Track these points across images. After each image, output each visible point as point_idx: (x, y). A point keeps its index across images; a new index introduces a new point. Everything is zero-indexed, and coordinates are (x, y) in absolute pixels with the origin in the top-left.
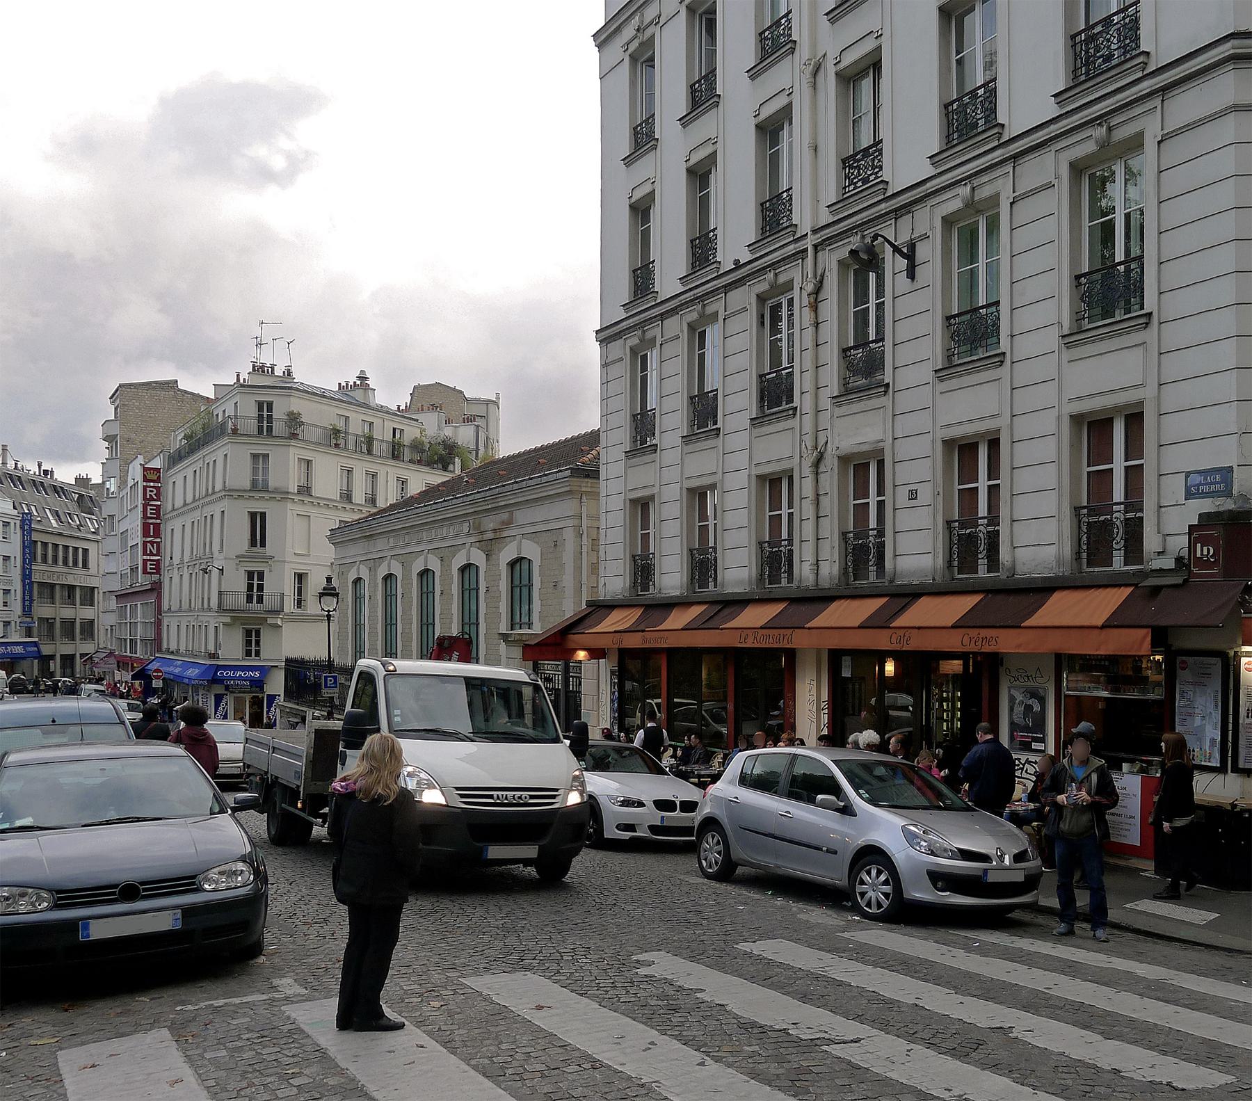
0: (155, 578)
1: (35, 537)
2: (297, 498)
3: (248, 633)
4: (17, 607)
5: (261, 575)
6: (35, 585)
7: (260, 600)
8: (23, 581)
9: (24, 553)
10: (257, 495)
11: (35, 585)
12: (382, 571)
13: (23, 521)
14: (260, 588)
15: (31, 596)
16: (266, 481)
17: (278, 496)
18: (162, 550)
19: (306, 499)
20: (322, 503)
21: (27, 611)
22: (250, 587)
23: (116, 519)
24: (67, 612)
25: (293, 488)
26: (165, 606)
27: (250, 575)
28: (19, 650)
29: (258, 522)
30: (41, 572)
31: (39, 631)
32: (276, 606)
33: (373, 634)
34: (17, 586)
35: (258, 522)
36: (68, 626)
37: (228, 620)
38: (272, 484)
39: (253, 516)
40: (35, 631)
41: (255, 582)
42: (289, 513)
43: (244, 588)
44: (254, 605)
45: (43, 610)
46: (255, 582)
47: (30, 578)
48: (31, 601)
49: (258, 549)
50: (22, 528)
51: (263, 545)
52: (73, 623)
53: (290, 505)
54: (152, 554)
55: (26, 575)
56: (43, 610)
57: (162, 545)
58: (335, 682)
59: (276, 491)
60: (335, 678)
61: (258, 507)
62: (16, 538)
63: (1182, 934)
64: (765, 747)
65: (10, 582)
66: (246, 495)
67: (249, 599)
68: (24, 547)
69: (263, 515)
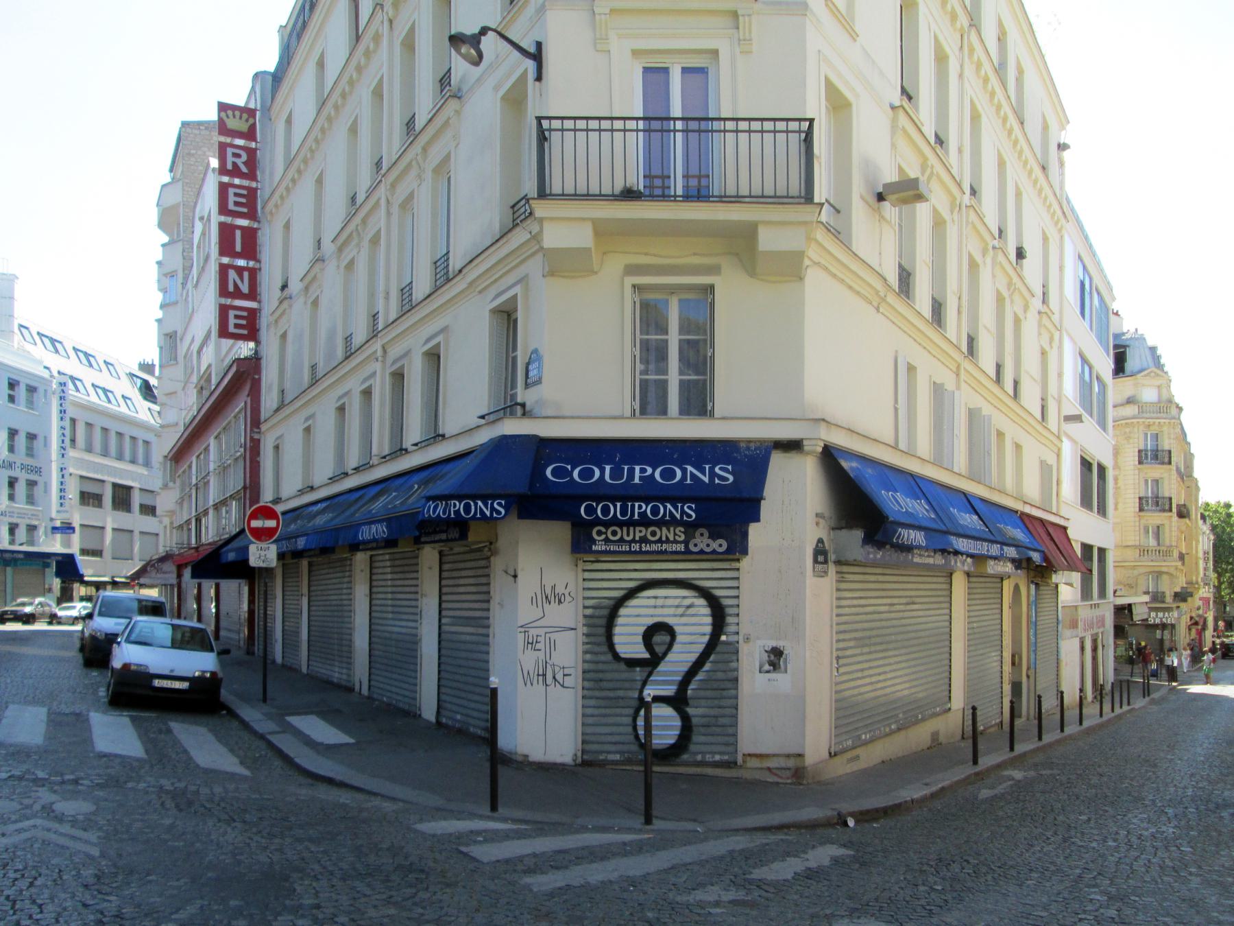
54: (238, 294)
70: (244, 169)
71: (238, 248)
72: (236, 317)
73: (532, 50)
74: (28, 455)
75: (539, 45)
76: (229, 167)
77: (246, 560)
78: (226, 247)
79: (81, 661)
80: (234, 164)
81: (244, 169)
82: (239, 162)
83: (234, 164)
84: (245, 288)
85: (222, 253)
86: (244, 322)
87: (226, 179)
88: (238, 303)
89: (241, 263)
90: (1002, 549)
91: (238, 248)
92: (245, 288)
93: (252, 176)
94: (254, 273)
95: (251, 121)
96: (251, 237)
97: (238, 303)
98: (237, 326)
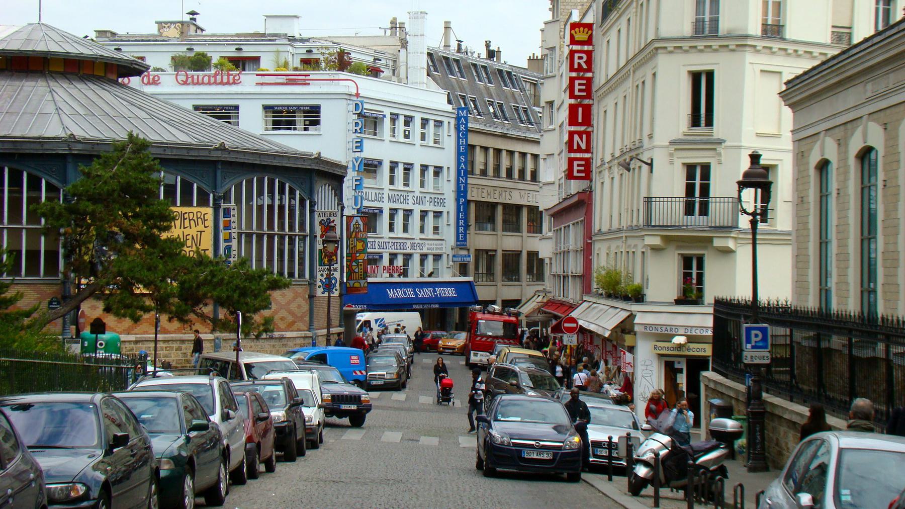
0: (584, 184)
1: (473, 140)
2: (760, 44)
3: (687, 262)
4: (449, 234)
5: (706, 170)
6: (473, 207)
7: (704, 211)
8: (457, 200)
9: (459, 163)
10: (700, 44)
11: (473, 207)
12: (855, 145)
13: (458, 119)
14: (705, 190)
15: (466, 220)
16: (715, 21)
17: (732, 44)
18: (594, 143)
19: (776, 45)
20: (801, 49)
21: (461, 241)
22: (690, 190)
23: (556, 106)
24: (511, 242)
25: (755, 28)
26: (596, 227)
27: (690, 169)
28: (450, 292)
29: (702, 85)
30: (482, 190)
31: (477, 268)
32: (727, 221)
33: (843, 257)
34: (450, 206)
35: (702, 85)
36: (511, 261)
37: (657, 241)
38: (724, 26)
39: (696, 77)
40: (472, 267)
41: (698, 180)
42: (748, 68)
43: (680, 190)
44: (696, 219)
45: (482, 240)
46: (698, 180)
47: (465, 196)
48: (467, 226)
49: (702, 130)
50: (457, 128)
51: (709, 123)
52: (518, 254)
53: (749, 57)
54: (579, 150)
55: (461, 192)
56: (482, 240)
57: (594, 136)
58: (764, 339)
59: (729, 37)
60: (764, 331)
61: (701, 63)
62: (450, 143)
63: (824, 184)
64: (808, 288)
65: (442, 202)
66: (686, 45)
67: (689, 211)
68: (459, 154)
69: (710, 75)
70: (585, 66)
71: (580, 120)
72: (578, 165)
73: (649, 162)
74: (434, 233)
75: (652, 160)
76: (576, 66)
77: (856, 397)
78: (573, 121)
79: (302, 458)
80: (579, 64)
81: (585, 66)
82: (581, 61)
83: (579, 64)
84: (583, 146)
85: (570, 124)
86: (582, 168)
87: (574, 74)
88: (578, 155)
89: (582, 128)
90: (435, 291)
91: (580, 120)
92: (583, 146)
93: (589, 70)
94: (589, 134)
95: (590, 32)
96: (587, 110)
97: (578, 155)
98: (579, 171)
